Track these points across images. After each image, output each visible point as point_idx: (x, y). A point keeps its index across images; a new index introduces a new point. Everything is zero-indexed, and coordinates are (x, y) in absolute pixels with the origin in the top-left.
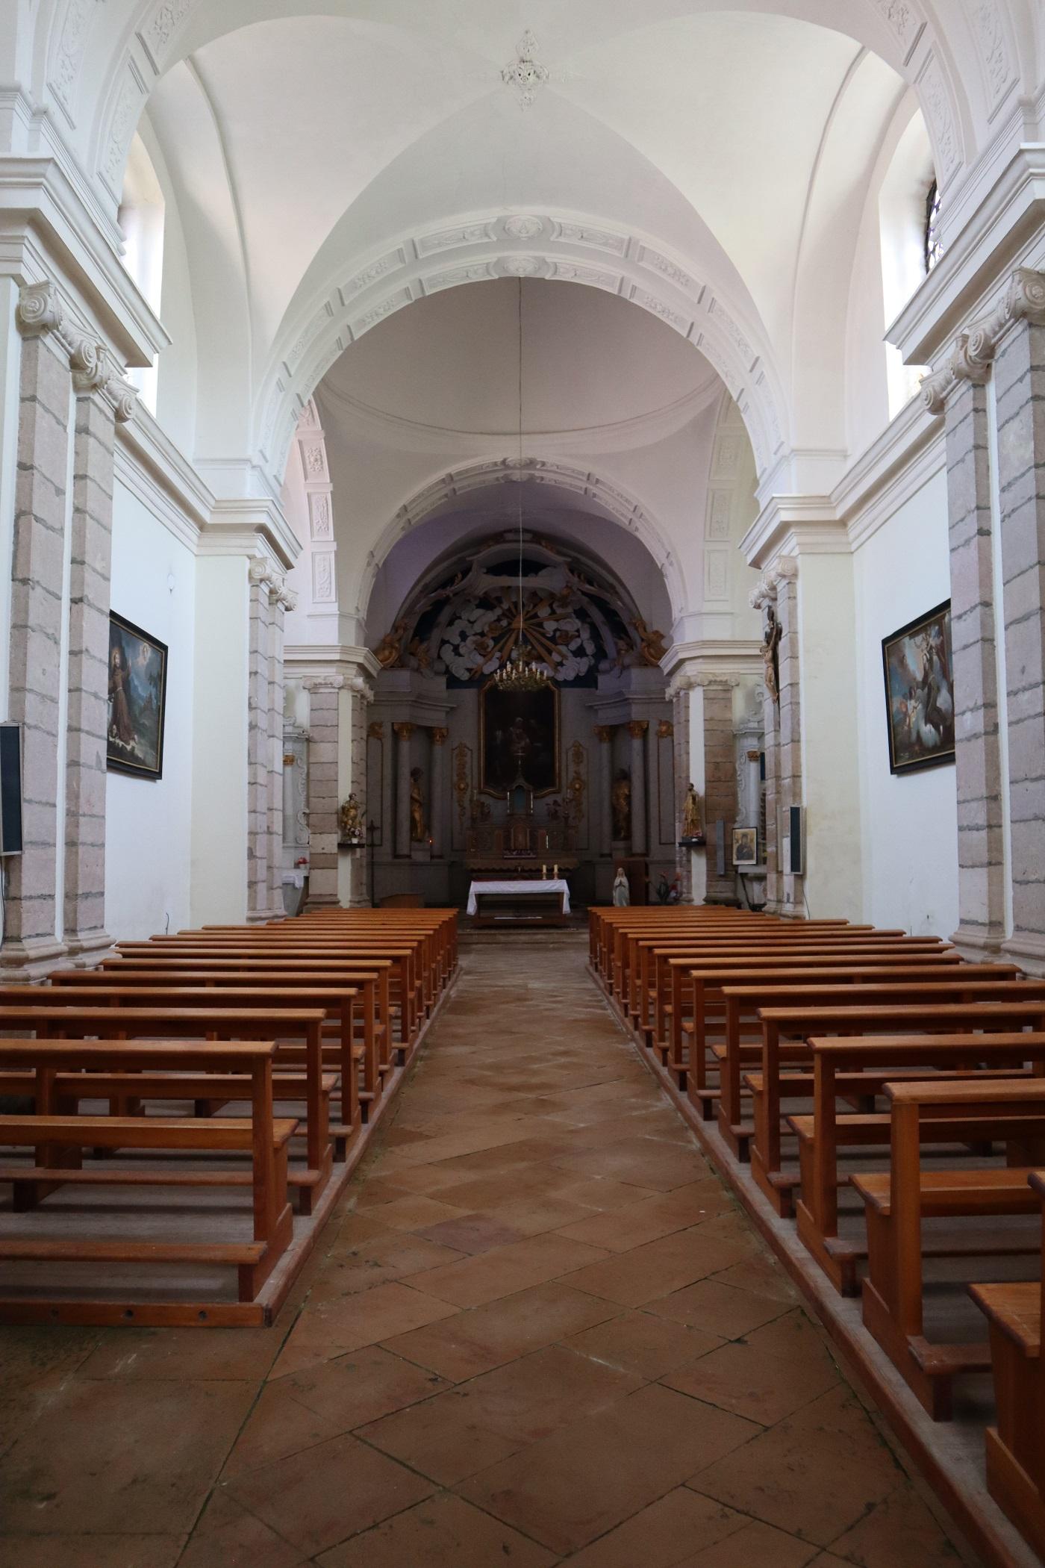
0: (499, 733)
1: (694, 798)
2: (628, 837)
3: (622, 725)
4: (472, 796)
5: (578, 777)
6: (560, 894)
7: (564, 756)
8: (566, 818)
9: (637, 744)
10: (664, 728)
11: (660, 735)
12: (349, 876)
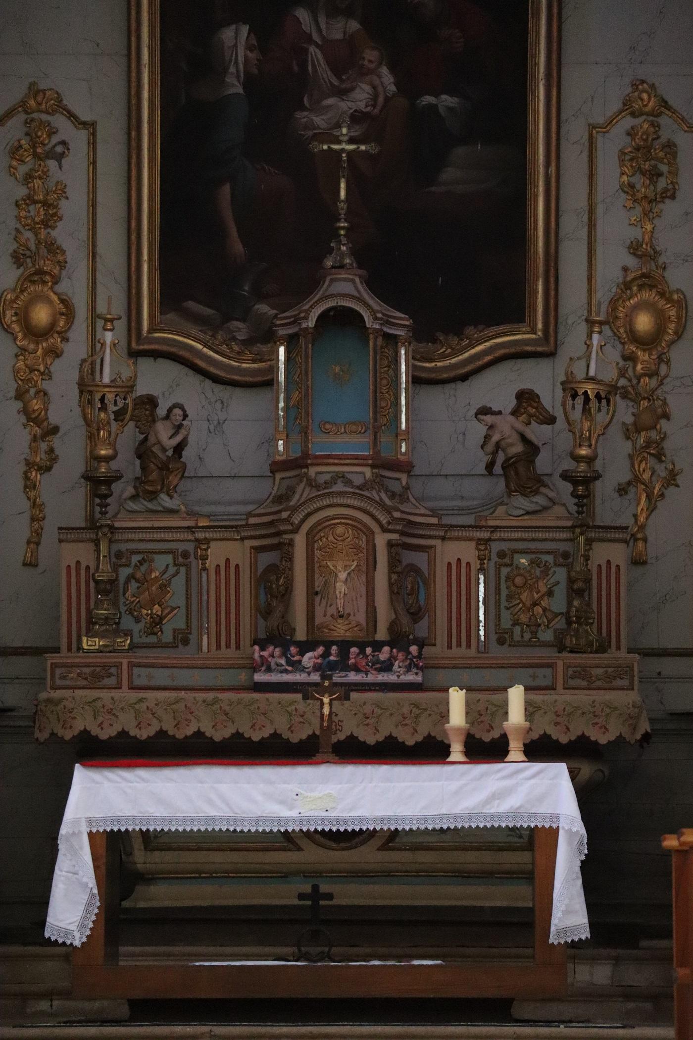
0: (236, 40)
4: (90, 368)
5: (646, 273)
6: (536, 841)
7: (574, 160)
8: (583, 483)
12: (143, 773)
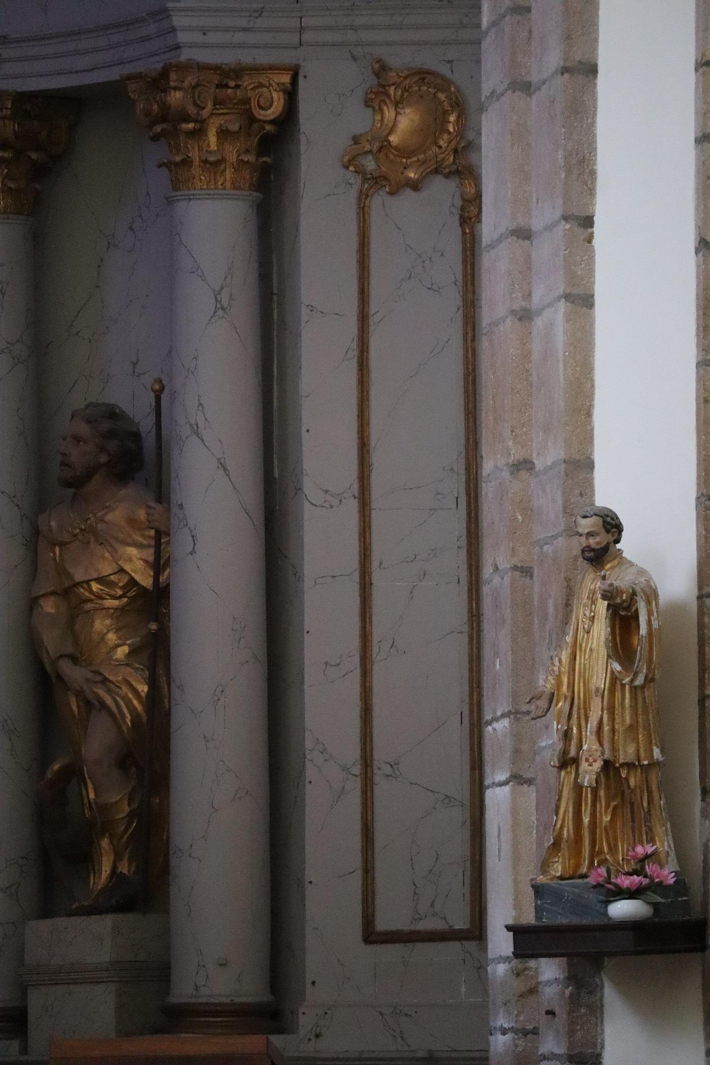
1: (623, 617)
2: (146, 890)
3: (108, 98)
9: (213, 226)
10: (405, 123)
11: (377, 172)
